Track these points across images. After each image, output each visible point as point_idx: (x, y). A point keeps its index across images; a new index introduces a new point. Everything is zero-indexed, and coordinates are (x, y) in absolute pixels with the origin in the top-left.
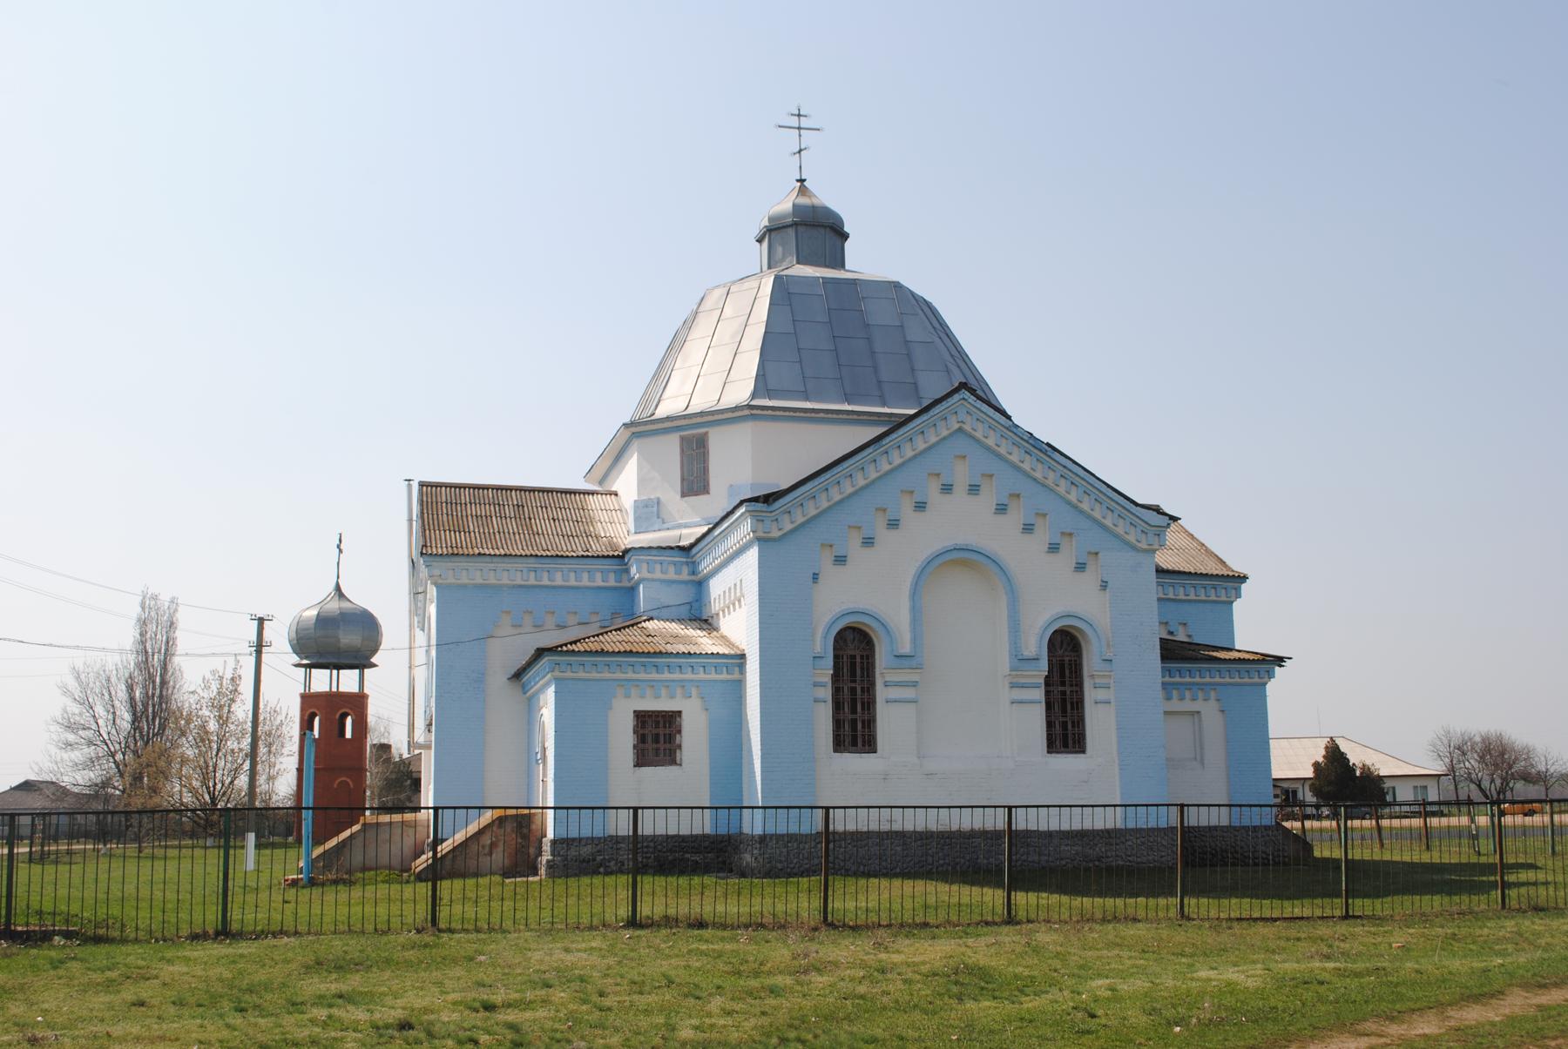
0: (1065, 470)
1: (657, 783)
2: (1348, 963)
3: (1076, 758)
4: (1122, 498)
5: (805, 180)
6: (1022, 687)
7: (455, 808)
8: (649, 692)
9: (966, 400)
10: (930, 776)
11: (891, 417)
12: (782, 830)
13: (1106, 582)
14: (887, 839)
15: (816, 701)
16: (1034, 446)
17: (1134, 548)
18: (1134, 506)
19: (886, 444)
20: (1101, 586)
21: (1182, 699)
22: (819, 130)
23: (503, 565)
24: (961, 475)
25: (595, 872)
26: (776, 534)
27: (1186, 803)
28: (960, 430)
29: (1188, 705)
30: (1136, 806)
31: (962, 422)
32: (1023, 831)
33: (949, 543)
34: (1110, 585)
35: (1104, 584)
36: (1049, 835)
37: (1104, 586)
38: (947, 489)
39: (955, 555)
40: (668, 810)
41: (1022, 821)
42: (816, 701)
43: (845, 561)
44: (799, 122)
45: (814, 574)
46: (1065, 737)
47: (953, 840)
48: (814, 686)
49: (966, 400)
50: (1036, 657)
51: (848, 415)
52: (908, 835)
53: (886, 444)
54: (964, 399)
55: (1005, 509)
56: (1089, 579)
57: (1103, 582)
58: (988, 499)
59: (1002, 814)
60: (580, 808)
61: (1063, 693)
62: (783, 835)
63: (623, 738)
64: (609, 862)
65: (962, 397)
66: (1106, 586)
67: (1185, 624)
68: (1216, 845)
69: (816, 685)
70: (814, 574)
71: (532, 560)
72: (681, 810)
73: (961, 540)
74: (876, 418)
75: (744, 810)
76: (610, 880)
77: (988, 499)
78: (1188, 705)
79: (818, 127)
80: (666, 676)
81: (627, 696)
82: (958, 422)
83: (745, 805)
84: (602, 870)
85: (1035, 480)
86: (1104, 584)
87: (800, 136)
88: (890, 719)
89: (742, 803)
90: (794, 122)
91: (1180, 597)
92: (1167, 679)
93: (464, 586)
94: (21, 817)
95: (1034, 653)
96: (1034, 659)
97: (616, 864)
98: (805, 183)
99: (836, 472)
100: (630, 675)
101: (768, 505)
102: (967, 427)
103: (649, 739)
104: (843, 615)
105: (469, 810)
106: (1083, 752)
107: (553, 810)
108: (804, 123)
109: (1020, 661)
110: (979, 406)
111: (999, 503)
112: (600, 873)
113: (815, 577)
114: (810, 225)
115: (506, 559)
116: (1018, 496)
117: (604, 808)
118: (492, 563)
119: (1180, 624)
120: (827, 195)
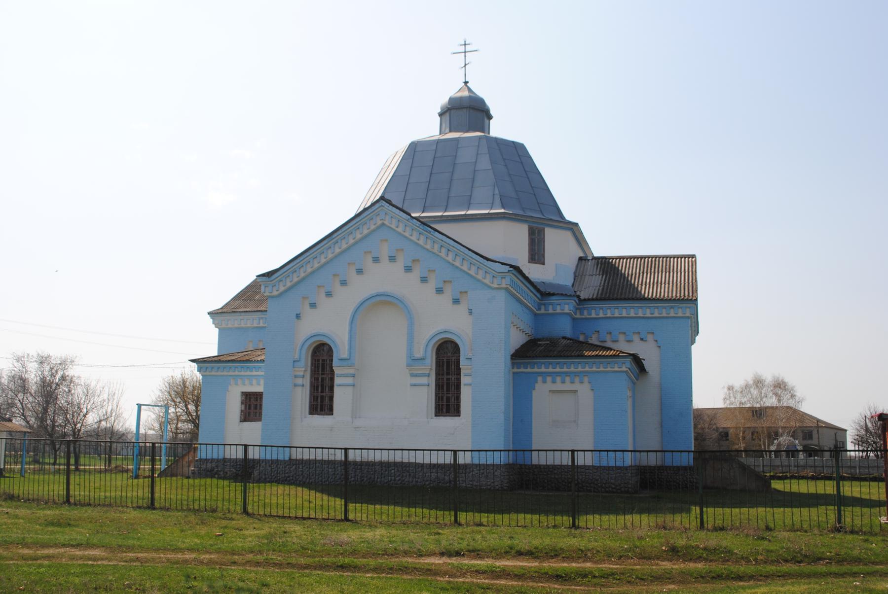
0: (443, 243)
1: (252, 433)
2: (38, 534)
3: (452, 419)
4: (479, 257)
5: (468, 82)
6: (416, 376)
7: (423, 450)
8: (239, 382)
9: (384, 206)
10: (357, 429)
11: (448, 217)
12: (268, 457)
13: (471, 310)
14: (324, 465)
15: (295, 385)
16: (423, 230)
17: (489, 287)
18: (486, 261)
19: (335, 237)
20: (469, 312)
21: (563, 382)
22: (476, 51)
23: (240, 317)
24: (385, 251)
25: (212, 477)
26: (275, 293)
27: (575, 449)
28: (383, 224)
29: (568, 386)
30: (368, 449)
31: (382, 219)
32: (448, 464)
33: (374, 292)
34: (473, 311)
35: (470, 311)
36: (422, 466)
37: (470, 312)
38: (376, 260)
39: (378, 299)
40: (555, 452)
41: (352, 456)
42: (295, 385)
43: (459, 302)
44: (465, 49)
45: (297, 314)
46: (448, 407)
47: (363, 467)
48: (295, 377)
49: (384, 206)
50: (422, 358)
51: (434, 218)
52: (227, 460)
53: (335, 237)
54: (382, 206)
55: (411, 269)
56: (462, 308)
57: (469, 310)
58: (399, 265)
59: (241, 449)
60: (438, 450)
61: (448, 379)
62: (269, 460)
63: (235, 406)
64: (220, 472)
65: (380, 205)
66: (471, 312)
67: (653, 333)
68: (687, 479)
69: (296, 377)
70: (297, 314)
71: (259, 313)
72: (356, 450)
73: (381, 290)
74: (433, 219)
75: (533, 452)
76: (221, 482)
77: (399, 265)
78: (568, 386)
79: (476, 49)
80: (254, 373)
81: (236, 384)
82: (381, 220)
83: (533, 449)
84: (216, 476)
85: (427, 250)
86: (470, 311)
87: (465, 56)
88: (341, 396)
89: (531, 448)
90: (462, 49)
91: (615, 316)
92: (516, 370)
93: (230, 329)
94: (459, 452)
95: (422, 355)
96: (421, 359)
97: (223, 473)
98: (468, 84)
99: (306, 256)
100: (237, 373)
101: (269, 277)
102: (386, 222)
103: (252, 407)
104: (311, 337)
105: (494, 452)
106: (459, 416)
107: (5, 440)
108: (468, 48)
109: (413, 360)
110: (390, 209)
111: (405, 266)
112: (215, 477)
113: (298, 316)
114: (458, 108)
115: (223, 315)
116: (418, 260)
117: (290, 447)
118: (241, 316)
119: (607, 333)
120: (480, 91)
